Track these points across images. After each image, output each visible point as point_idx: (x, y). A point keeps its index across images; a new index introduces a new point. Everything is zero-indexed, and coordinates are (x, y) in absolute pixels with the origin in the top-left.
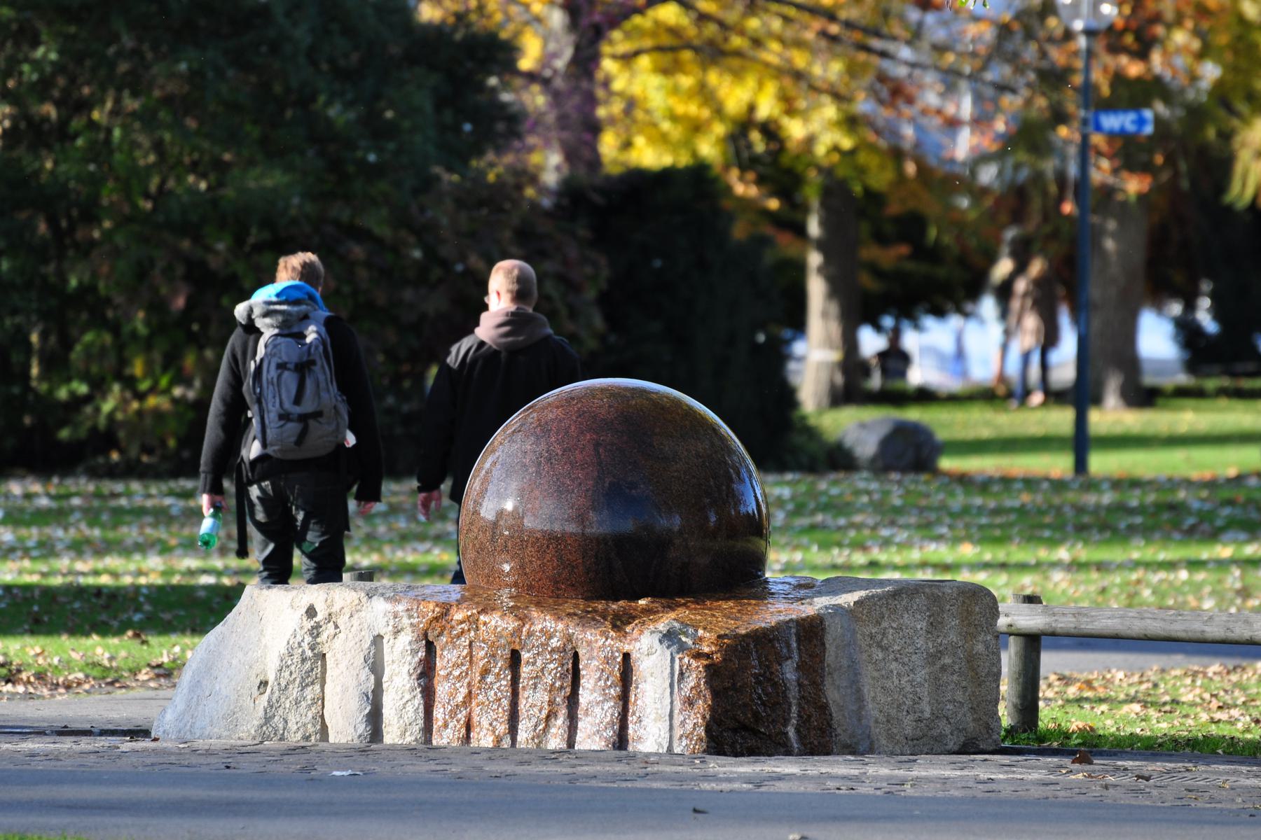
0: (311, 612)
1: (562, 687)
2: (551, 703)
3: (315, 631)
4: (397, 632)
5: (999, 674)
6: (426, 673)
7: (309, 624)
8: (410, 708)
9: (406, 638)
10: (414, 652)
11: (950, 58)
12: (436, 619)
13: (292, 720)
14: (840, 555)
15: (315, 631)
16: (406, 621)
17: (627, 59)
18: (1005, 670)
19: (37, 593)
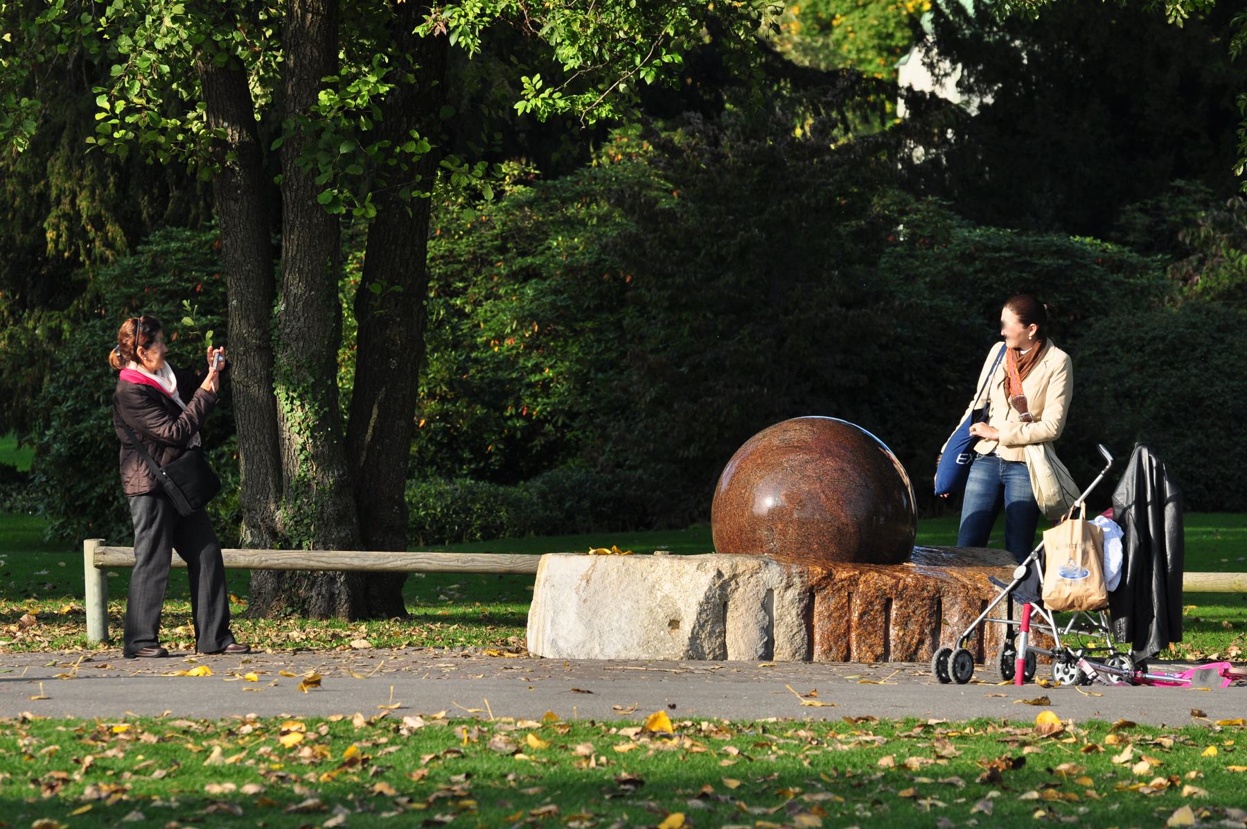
0: (720, 574)
1: (930, 623)
2: (922, 633)
3: (723, 587)
4: (788, 587)
5: (279, 573)
6: (807, 614)
7: (719, 583)
8: (798, 638)
9: (792, 594)
10: (801, 600)
11: (1148, 350)
12: (824, 578)
13: (706, 645)
14: (578, 210)
15: (723, 587)
16: (797, 580)
17: (845, 59)
18: (370, 431)
19: (422, 544)
